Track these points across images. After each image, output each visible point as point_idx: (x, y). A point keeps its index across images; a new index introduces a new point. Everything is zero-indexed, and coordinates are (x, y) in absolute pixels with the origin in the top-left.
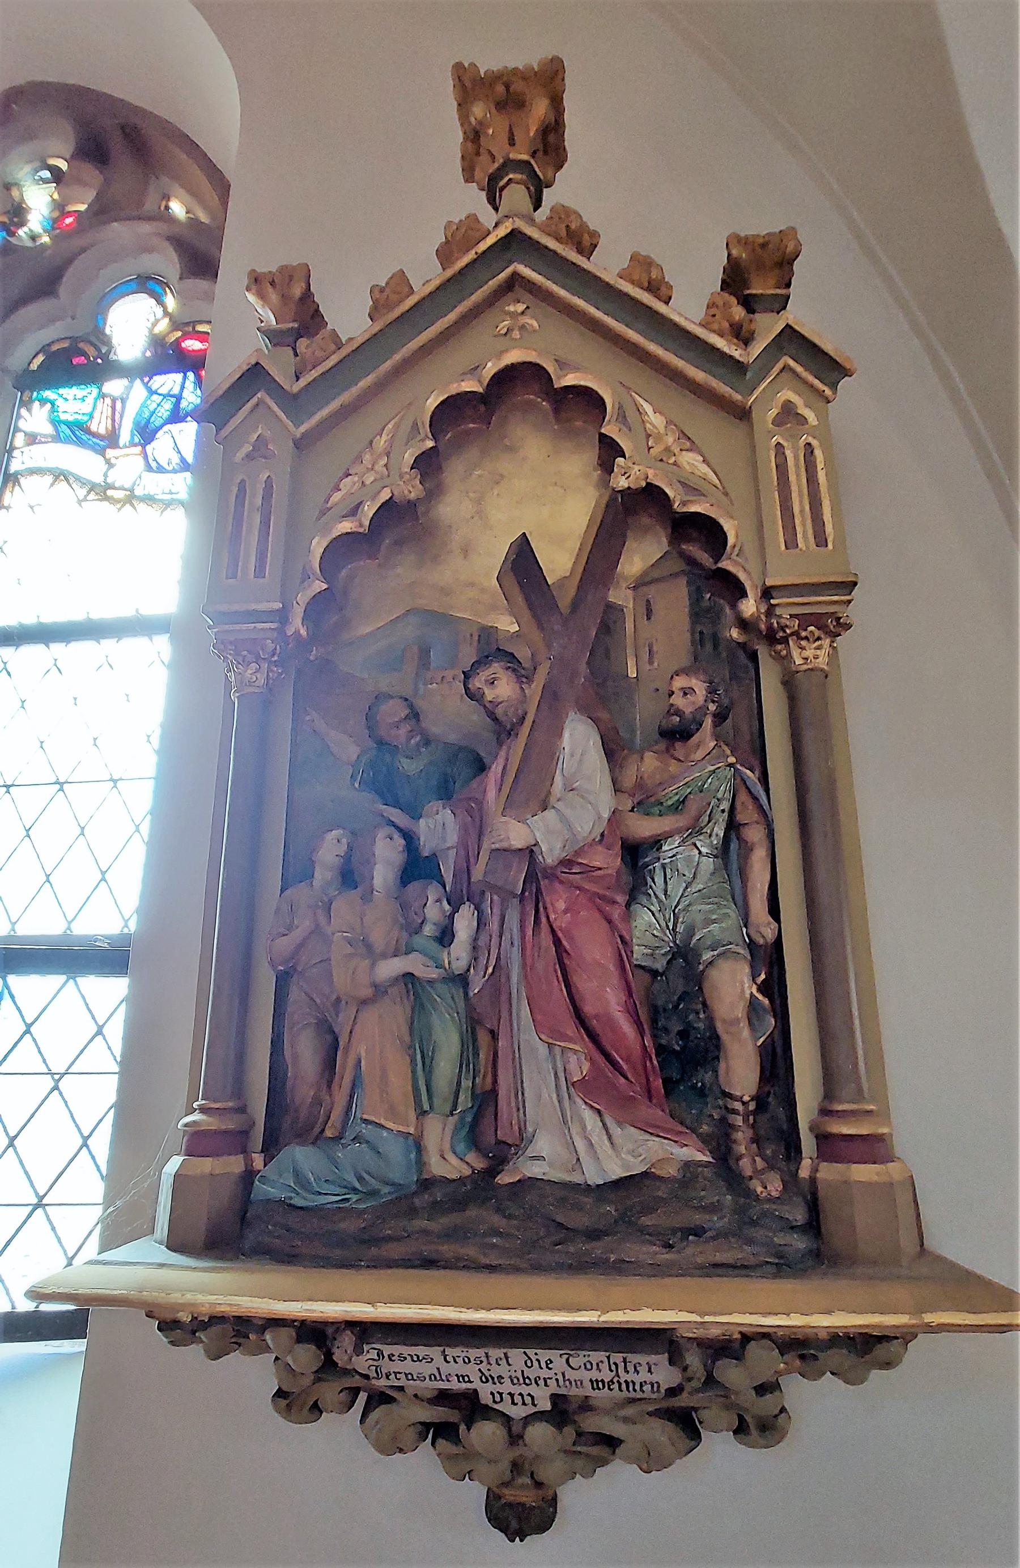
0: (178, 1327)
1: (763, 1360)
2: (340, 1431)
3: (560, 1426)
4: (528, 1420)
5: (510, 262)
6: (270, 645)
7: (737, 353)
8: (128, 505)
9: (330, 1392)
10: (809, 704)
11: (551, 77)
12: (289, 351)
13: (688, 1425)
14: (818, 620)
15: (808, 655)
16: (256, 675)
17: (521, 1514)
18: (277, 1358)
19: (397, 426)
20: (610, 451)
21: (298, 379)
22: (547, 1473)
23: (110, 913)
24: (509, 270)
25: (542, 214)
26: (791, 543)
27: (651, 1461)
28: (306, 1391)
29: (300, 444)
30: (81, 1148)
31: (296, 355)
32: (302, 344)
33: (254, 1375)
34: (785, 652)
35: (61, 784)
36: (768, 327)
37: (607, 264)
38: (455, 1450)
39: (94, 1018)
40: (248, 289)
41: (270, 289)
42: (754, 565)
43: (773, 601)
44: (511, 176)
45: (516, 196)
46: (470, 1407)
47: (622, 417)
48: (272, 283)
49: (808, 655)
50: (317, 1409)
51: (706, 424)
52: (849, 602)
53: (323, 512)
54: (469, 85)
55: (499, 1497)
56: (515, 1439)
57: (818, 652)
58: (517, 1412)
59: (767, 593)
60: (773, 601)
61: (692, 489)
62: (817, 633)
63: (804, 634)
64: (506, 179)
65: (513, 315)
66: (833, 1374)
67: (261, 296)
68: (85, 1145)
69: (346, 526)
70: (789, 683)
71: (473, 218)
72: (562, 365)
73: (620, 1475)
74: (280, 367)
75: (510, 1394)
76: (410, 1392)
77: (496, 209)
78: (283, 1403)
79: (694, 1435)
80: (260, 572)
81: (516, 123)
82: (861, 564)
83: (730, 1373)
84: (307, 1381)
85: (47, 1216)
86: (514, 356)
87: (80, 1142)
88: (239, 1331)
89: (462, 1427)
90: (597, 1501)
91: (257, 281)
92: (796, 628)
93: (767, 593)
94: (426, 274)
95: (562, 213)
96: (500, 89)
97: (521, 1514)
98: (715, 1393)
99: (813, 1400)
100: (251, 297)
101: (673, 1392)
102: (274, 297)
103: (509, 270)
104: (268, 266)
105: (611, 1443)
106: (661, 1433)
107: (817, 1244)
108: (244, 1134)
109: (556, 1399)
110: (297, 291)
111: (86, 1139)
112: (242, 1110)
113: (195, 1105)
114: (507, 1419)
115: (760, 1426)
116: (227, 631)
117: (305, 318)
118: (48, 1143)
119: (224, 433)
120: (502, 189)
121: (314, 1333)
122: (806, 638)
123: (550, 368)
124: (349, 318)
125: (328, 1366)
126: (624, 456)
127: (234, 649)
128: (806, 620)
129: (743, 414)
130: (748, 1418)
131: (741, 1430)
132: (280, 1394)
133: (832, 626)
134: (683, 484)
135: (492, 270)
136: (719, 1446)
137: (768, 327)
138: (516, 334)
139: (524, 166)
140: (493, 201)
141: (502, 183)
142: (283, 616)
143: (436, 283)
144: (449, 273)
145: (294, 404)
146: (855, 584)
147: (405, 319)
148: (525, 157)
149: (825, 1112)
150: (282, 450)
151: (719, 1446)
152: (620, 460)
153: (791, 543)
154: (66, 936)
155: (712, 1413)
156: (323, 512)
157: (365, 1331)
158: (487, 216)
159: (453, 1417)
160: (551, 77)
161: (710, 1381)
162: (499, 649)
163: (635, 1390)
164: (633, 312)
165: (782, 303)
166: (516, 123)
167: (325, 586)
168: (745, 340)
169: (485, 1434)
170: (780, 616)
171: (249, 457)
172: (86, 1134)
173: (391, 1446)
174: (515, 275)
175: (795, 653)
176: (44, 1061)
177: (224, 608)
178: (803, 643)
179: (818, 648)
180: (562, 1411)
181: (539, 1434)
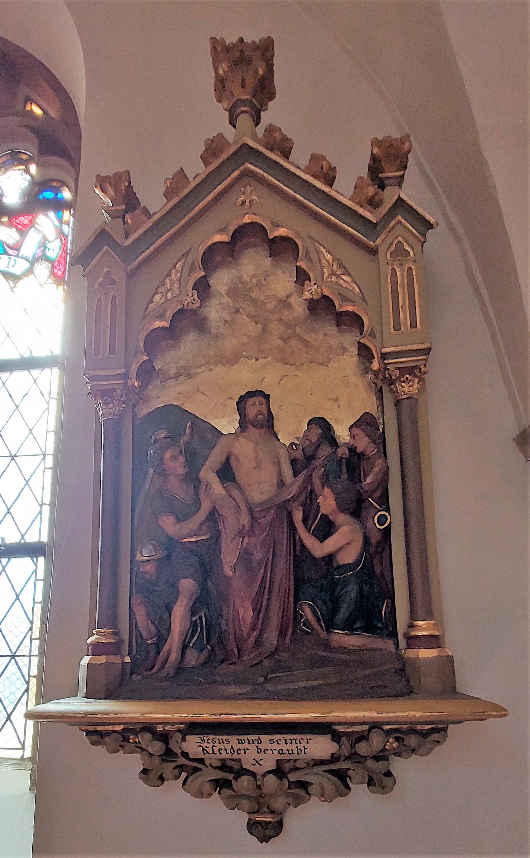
1: (377, 741)
4: (264, 775)
7: (367, 215)
9: (169, 769)
11: (266, 48)
12: (120, 220)
14: (411, 370)
15: (407, 389)
17: (267, 829)
21: (127, 238)
23: (39, 533)
24: (242, 168)
25: (260, 131)
26: (397, 327)
29: (131, 275)
30: (15, 600)
32: (128, 218)
35: (13, 457)
38: (231, 792)
39: (13, 518)
43: (386, 362)
44: (243, 109)
45: (245, 121)
49: (407, 389)
50: (162, 779)
51: (352, 256)
53: (144, 316)
54: (220, 50)
60: (386, 362)
61: (345, 299)
67: (103, 190)
68: (17, 598)
69: (158, 324)
71: (221, 136)
74: (116, 230)
76: (207, 762)
77: (235, 127)
80: (112, 351)
81: (248, 72)
83: (362, 748)
85: (10, 452)
89: (234, 782)
90: (304, 820)
91: (102, 182)
92: (398, 376)
93: (384, 356)
94: (196, 170)
95: (271, 129)
96: (237, 54)
97: (267, 829)
100: (97, 191)
101: (334, 758)
103: (242, 168)
104: (108, 171)
105: (304, 785)
106: (329, 783)
107: (402, 681)
108: (119, 644)
111: (18, 596)
112: (116, 634)
114: (253, 775)
115: (381, 781)
117: (128, 201)
120: (237, 117)
122: (404, 382)
125: (168, 755)
129: (374, 252)
130: (375, 777)
131: (371, 782)
132: (145, 771)
135: (230, 164)
136: (359, 790)
142: (126, 376)
143: (203, 177)
145: (127, 254)
146: (430, 349)
149: (411, 626)
150: (120, 278)
151: (359, 790)
153: (397, 327)
155: (357, 774)
158: (230, 133)
160: (266, 48)
161: (354, 756)
163: (219, 740)
165: (400, 181)
166: (248, 72)
167: (148, 358)
171: (101, 284)
172: (18, 593)
174: (246, 169)
175: (399, 388)
177: (92, 373)
180: (279, 771)
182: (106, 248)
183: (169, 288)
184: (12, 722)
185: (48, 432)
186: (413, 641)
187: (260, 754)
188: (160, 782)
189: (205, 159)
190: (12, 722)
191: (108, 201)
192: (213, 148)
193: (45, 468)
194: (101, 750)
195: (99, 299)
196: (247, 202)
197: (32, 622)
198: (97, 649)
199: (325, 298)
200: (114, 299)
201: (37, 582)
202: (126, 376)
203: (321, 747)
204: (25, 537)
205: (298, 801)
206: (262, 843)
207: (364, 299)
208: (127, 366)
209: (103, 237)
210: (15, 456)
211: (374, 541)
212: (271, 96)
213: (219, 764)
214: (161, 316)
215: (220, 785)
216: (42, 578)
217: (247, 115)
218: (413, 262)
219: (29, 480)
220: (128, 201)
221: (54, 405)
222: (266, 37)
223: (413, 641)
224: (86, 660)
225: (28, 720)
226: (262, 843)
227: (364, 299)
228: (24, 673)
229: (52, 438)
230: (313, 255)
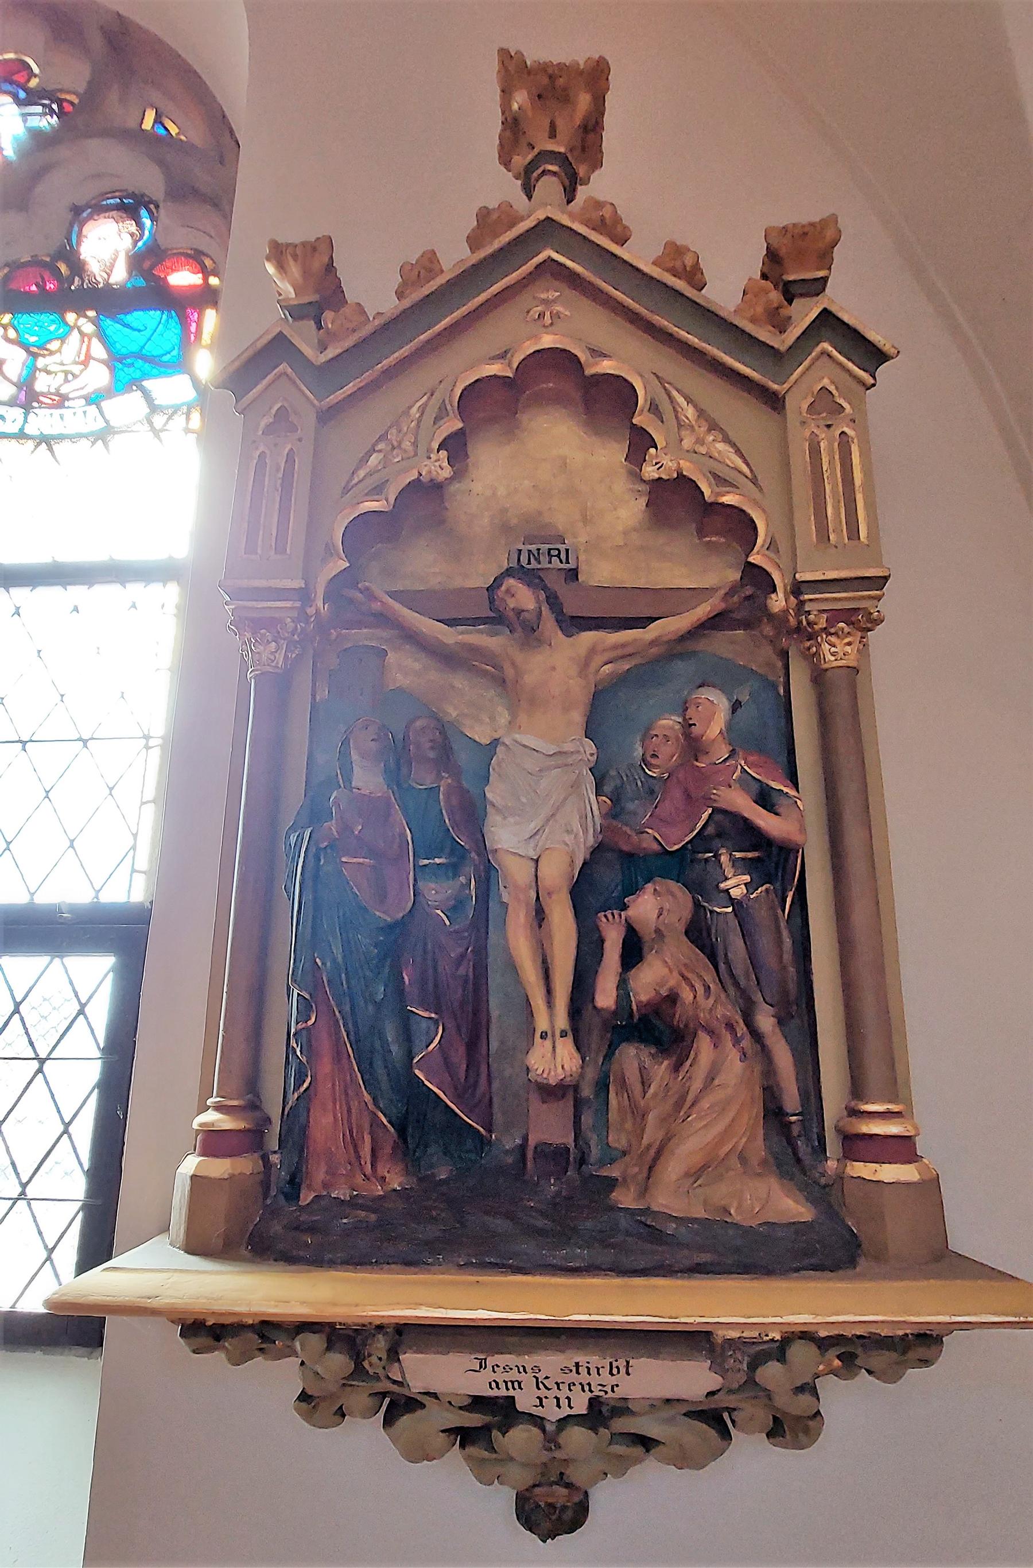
0: (205, 1331)
2: (364, 1436)
3: (594, 1429)
4: (564, 1422)
5: (544, 248)
6: (291, 625)
8: (100, 441)
9: (359, 1397)
10: (841, 702)
13: (715, 1418)
14: (848, 615)
15: (836, 652)
16: (273, 654)
17: (552, 1511)
18: (302, 1363)
19: (423, 410)
20: (640, 444)
22: (577, 1475)
23: (127, 888)
27: (685, 1460)
28: (332, 1397)
29: (327, 416)
31: (319, 327)
33: (278, 1379)
34: (814, 649)
36: (804, 313)
37: (641, 253)
40: (268, 259)
41: (292, 262)
42: (785, 561)
45: (549, 187)
46: (500, 1411)
47: (654, 408)
48: (295, 257)
49: (836, 652)
50: (341, 1413)
52: (879, 598)
53: (346, 490)
54: (513, 69)
55: (528, 1499)
56: (552, 1441)
57: (848, 649)
58: (552, 1414)
59: (797, 589)
60: (801, 598)
61: (719, 480)
62: (847, 629)
63: (832, 630)
64: (540, 171)
65: (546, 302)
66: (870, 1372)
67: (281, 267)
68: (66, 1131)
70: (819, 678)
72: (598, 353)
73: (652, 1476)
75: (556, 1397)
77: (530, 198)
78: (304, 1405)
79: (726, 1435)
81: (557, 118)
82: (892, 560)
83: (771, 1372)
84: (333, 1387)
86: (547, 341)
87: (61, 1128)
88: (267, 1334)
89: (495, 1433)
90: (628, 1501)
91: (279, 253)
93: (797, 589)
94: (455, 256)
95: (599, 205)
97: (552, 1511)
98: (761, 1396)
99: (847, 1403)
100: (271, 269)
102: (294, 269)
104: (295, 234)
105: (646, 1443)
109: (594, 1403)
110: (318, 263)
113: (209, 1102)
114: (538, 1421)
115: (791, 1428)
116: (245, 607)
117: (323, 293)
118: (32, 1131)
119: (821, 274)
121: (346, 1338)
122: (835, 634)
123: (583, 357)
124: (374, 291)
126: (657, 448)
127: (253, 625)
128: (836, 616)
129: (774, 401)
133: (861, 622)
134: (716, 476)
135: (508, 260)
137: (804, 313)
138: (547, 319)
139: (562, 159)
140: (528, 190)
141: (535, 175)
144: (482, 254)
146: (886, 578)
147: (442, 303)
148: (562, 150)
152: (652, 451)
154: (31, 903)
156: (346, 490)
157: (405, 1334)
159: (484, 1424)
160: (597, 76)
161: (751, 1382)
162: (487, 589)
164: (665, 302)
166: (557, 118)
168: (781, 326)
169: (519, 1439)
170: (809, 613)
173: (418, 1453)
176: (31, 1044)
178: (833, 639)
179: (849, 644)
180: (599, 1414)
181: (577, 1437)
182: (284, 367)
183: (395, 444)
184: (86, 1018)
185: (143, 803)
186: (856, 1146)
187: (549, 1385)
188: (337, 1418)
189: (474, 241)
190: (86, 1018)
191: (288, 290)
192: (488, 222)
193: (134, 871)
194: (217, 1358)
195: (262, 455)
196: (548, 314)
197: (135, 836)
198: (213, 1143)
199: (683, 481)
200: (290, 459)
201: (135, 874)
202: (305, 595)
203: (693, 1379)
204: (100, 895)
205: (621, 1466)
206: (544, 1541)
207: (754, 481)
208: (308, 577)
209: (277, 348)
210: (37, 1058)
211: (792, 997)
212: (597, 163)
213: (467, 1401)
214: (378, 490)
215: (465, 1436)
216: (151, 798)
217: (554, 179)
218: (851, 424)
219: (61, 1136)
220: (323, 293)
221: (155, 756)
222: (596, 57)
223: (856, 1146)
224: (191, 1164)
225: (170, 594)
226: (544, 1541)
227: (754, 481)
228: (83, 1161)
229: (150, 811)
230: (665, 407)
